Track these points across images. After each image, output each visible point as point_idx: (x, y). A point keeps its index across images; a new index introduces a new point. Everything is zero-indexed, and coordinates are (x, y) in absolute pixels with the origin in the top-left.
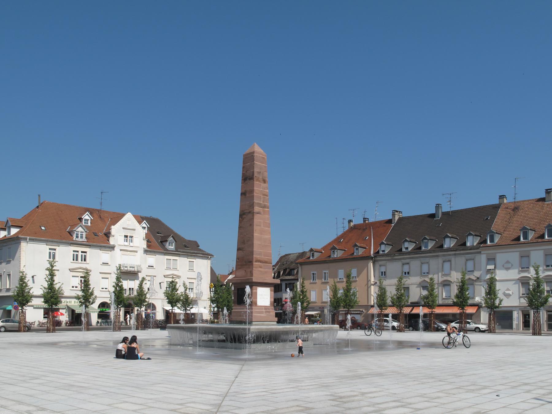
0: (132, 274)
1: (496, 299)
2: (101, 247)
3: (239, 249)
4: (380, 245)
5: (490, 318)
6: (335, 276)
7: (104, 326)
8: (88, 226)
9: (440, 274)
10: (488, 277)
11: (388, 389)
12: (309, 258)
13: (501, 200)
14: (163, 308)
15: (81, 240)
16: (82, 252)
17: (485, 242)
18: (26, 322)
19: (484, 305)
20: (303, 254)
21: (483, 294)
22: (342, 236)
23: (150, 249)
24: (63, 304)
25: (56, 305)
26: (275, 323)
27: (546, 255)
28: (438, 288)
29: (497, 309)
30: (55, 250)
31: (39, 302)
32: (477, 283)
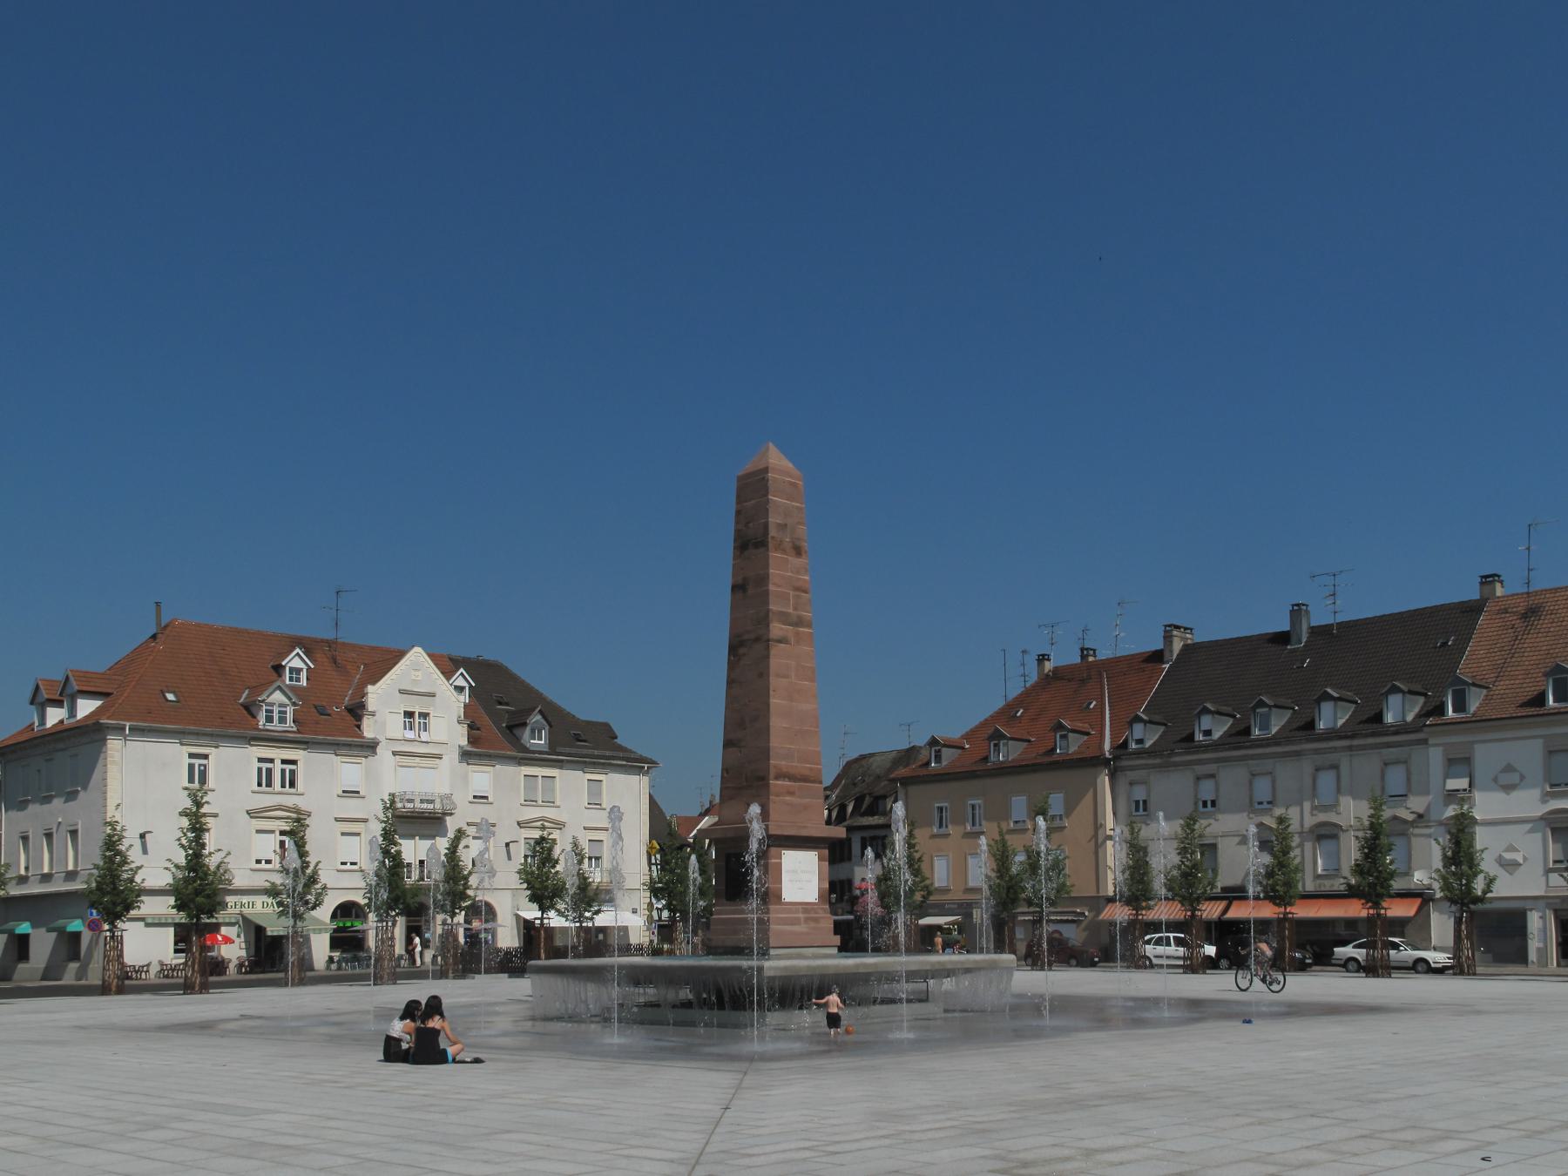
0: (426, 822)
1: (1475, 875)
2: (336, 747)
3: (728, 744)
4: (1131, 724)
5: (1457, 932)
6: (1004, 813)
7: (348, 969)
8: (302, 688)
9: (1307, 805)
10: (1451, 811)
11: (1160, 1140)
12: (928, 763)
13: (1487, 588)
14: (517, 916)
15: (280, 727)
16: (284, 762)
17: (1440, 710)
18: (123, 964)
19: (1439, 895)
20: (912, 752)
21: (1437, 863)
22: (1020, 701)
23: (478, 749)
24: (230, 911)
25: (210, 913)
26: (835, 951)
27: (1550, 752)
28: (1301, 845)
29: (1480, 906)
30: (206, 757)
31: (163, 906)
32: (1417, 831)
